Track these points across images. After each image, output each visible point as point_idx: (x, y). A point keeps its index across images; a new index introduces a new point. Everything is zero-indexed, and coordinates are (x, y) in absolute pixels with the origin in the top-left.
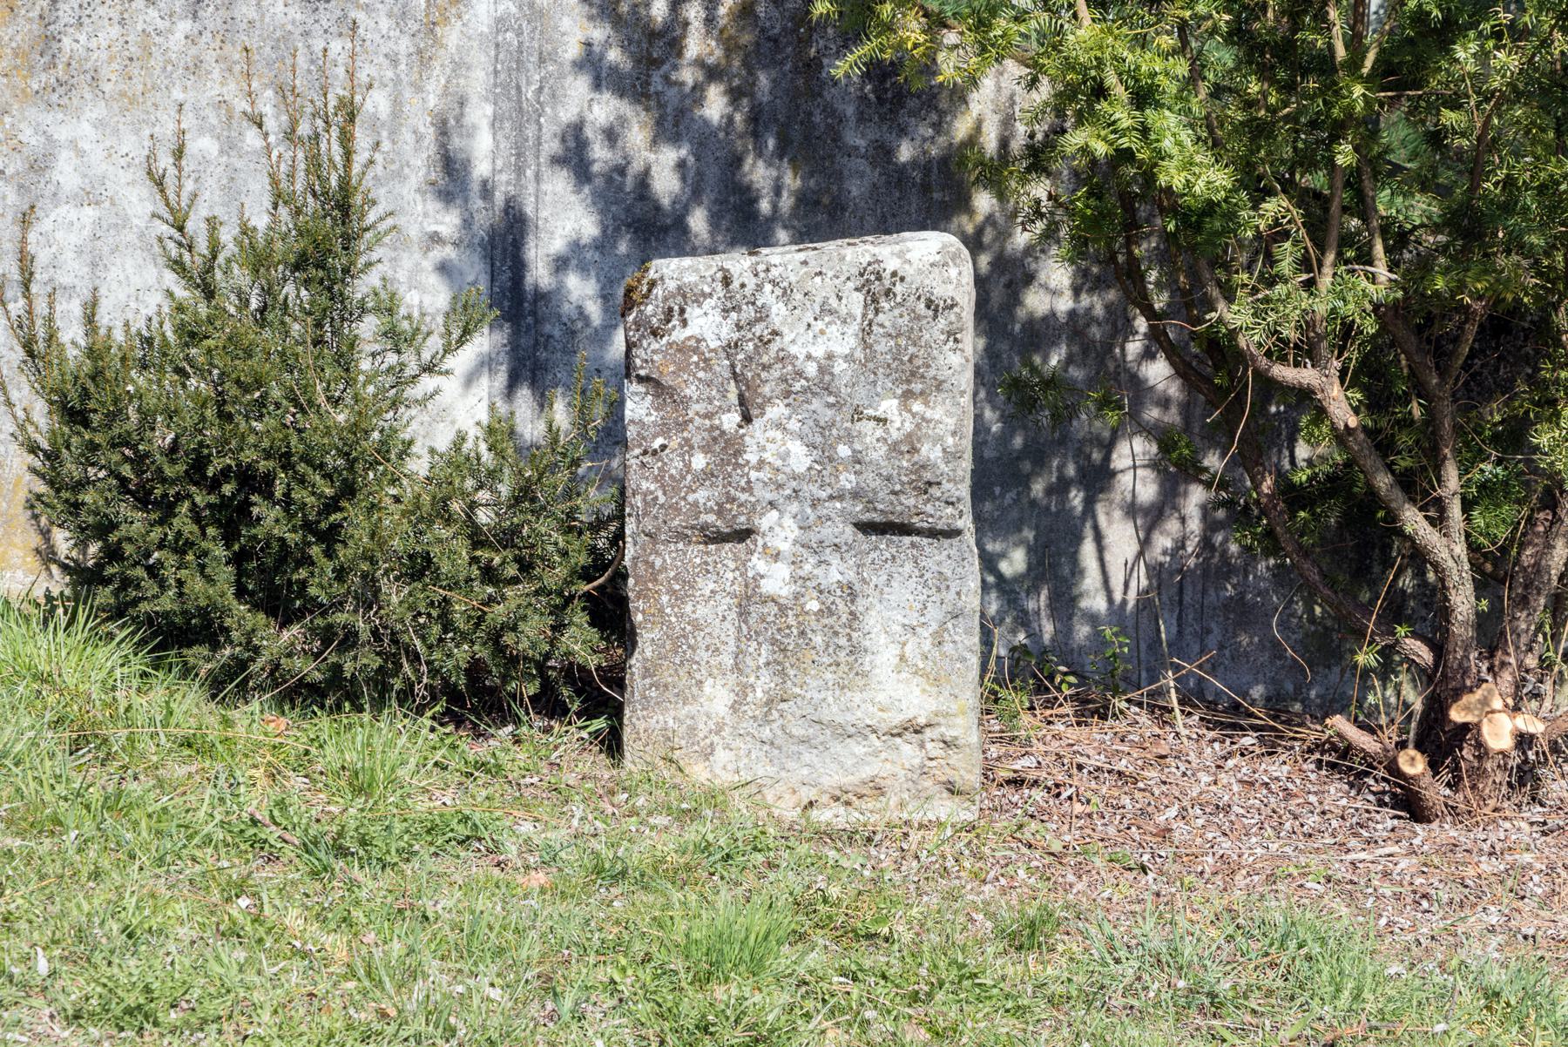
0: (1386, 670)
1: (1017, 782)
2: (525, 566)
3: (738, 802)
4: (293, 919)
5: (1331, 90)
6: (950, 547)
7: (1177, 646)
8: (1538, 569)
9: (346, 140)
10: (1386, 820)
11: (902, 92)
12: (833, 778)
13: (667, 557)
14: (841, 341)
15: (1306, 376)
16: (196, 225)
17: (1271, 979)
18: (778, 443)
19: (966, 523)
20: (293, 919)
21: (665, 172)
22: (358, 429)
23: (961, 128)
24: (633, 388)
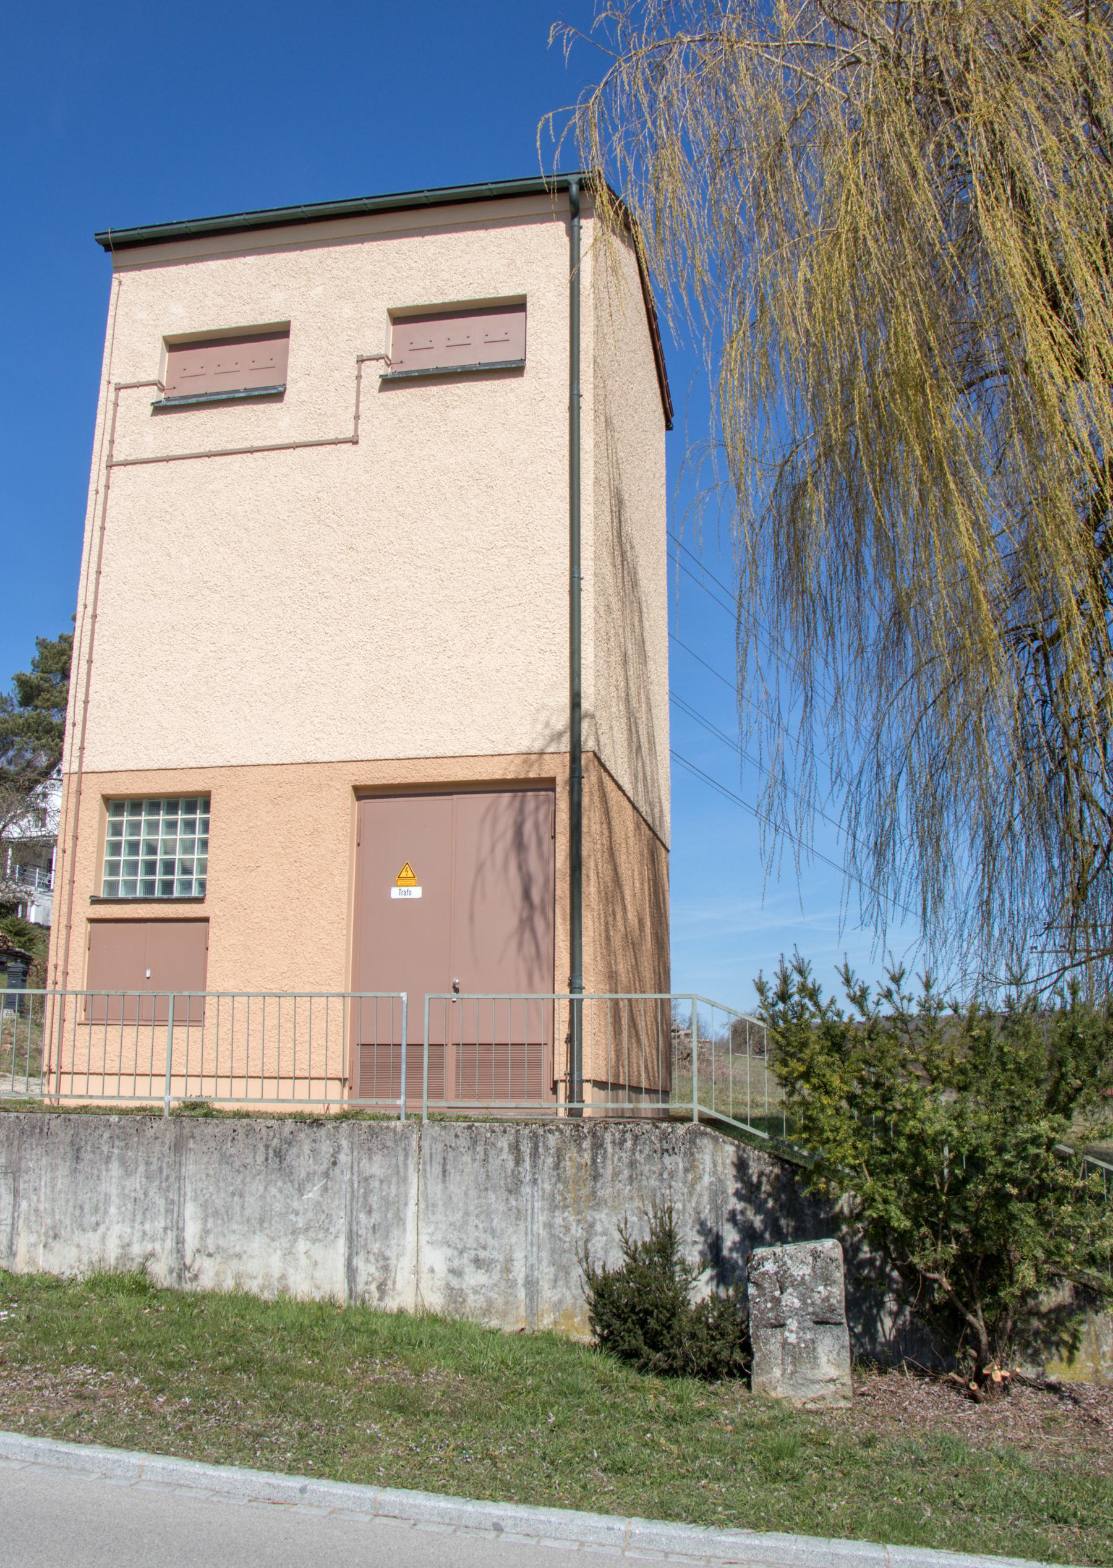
0: (964, 1358)
1: (863, 1394)
2: (722, 1335)
3: (785, 1403)
4: (663, 1441)
5: (936, 1196)
6: (840, 1328)
7: (906, 1353)
8: (1004, 1328)
9: (670, 1218)
10: (967, 1403)
11: (822, 1200)
12: (811, 1395)
13: (762, 1332)
14: (806, 1270)
15: (936, 1276)
16: (631, 1241)
17: (939, 1455)
18: (791, 1300)
19: (844, 1321)
20: (663, 1441)
21: (758, 1221)
22: (675, 1297)
23: (837, 1208)
24: (750, 1285)
